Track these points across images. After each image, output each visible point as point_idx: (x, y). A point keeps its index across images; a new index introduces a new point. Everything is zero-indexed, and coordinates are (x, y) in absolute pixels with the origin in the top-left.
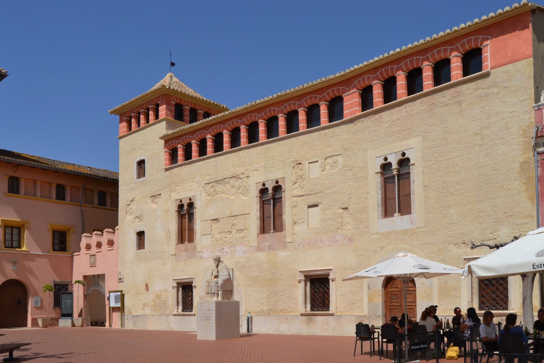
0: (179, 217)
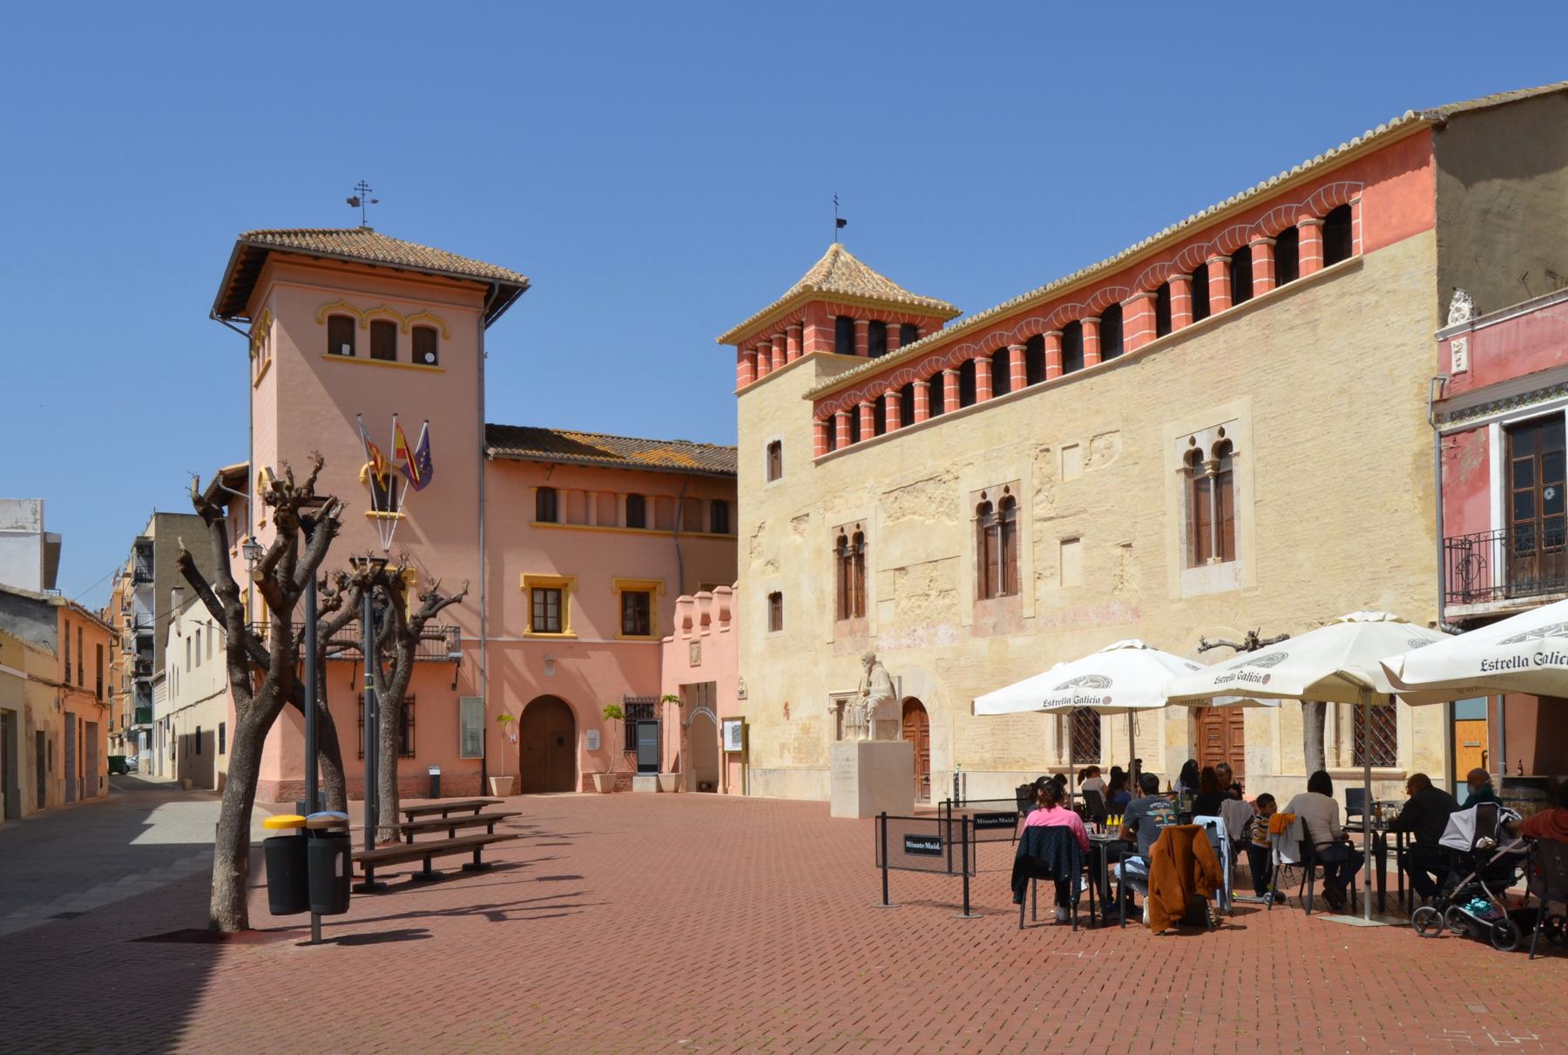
0: (839, 564)
